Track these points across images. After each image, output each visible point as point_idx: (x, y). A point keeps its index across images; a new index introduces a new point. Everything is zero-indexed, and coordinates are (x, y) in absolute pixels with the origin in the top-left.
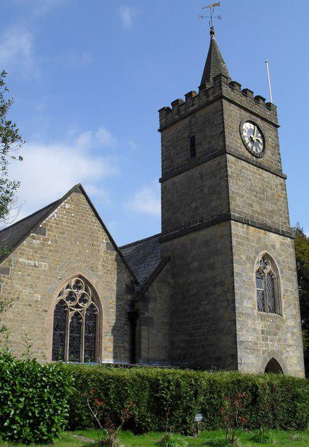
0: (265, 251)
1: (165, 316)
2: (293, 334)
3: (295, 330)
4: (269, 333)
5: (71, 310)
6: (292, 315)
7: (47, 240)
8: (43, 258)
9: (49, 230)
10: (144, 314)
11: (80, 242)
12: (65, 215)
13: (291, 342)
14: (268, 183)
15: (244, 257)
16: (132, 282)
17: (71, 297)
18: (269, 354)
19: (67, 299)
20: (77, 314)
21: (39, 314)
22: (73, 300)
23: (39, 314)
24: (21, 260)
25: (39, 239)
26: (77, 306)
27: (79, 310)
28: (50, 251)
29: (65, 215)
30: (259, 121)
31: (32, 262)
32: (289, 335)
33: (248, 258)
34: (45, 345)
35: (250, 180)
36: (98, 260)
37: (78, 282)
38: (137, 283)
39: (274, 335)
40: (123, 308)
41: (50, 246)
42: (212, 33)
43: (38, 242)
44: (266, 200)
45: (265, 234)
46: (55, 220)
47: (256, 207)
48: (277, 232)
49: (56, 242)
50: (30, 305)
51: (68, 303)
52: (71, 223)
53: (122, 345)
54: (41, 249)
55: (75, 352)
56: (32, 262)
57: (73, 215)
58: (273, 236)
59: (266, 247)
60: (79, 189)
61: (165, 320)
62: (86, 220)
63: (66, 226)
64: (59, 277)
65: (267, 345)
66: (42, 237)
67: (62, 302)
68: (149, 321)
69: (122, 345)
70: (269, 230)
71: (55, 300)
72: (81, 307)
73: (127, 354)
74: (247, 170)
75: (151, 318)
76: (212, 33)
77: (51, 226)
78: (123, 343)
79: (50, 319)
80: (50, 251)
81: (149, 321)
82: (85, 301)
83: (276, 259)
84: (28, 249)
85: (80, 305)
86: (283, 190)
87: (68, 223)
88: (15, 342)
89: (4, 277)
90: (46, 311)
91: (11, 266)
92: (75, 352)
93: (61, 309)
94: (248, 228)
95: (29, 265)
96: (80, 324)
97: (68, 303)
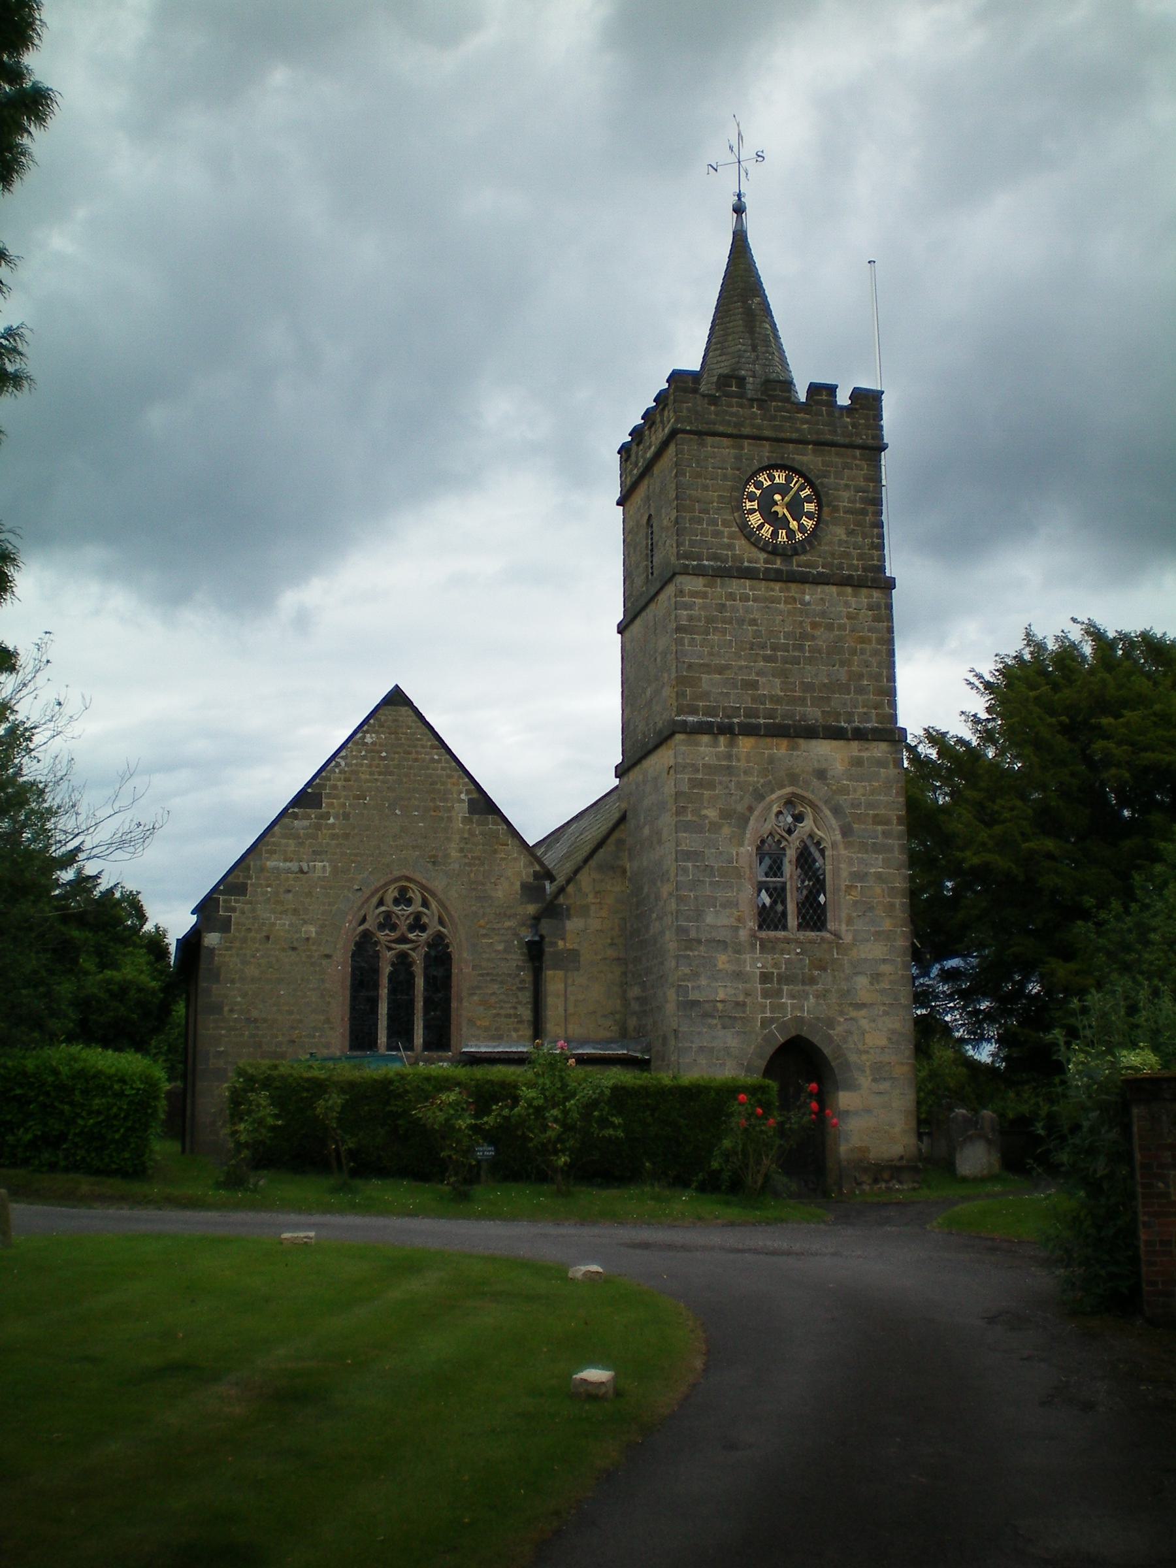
0: (788, 790)
1: (612, 944)
3: (886, 968)
4: (784, 979)
5: (390, 949)
7: (327, 816)
8: (317, 854)
9: (329, 796)
10: (554, 944)
12: (364, 757)
13: (864, 996)
14: (823, 614)
15: (712, 814)
16: (536, 875)
17: (388, 922)
19: (381, 927)
20: (403, 957)
21: (313, 964)
22: (394, 927)
23: (313, 964)
24: (270, 864)
25: (308, 817)
26: (403, 940)
27: (407, 946)
29: (364, 757)
30: (808, 458)
31: (294, 866)
33: (726, 814)
34: (328, 1021)
35: (753, 622)
36: (449, 839)
37: (403, 891)
38: (550, 876)
39: (803, 983)
40: (516, 935)
41: (333, 826)
42: (739, 209)
43: (306, 823)
44: (810, 661)
48: (836, 734)
49: (346, 816)
50: (294, 949)
51: (382, 936)
52: (380, 773)
53: (512, 1012)
54: (315, 837)
55: (401, 1031)
56: (294, 866)
57: (384, 754)
58: (824, 751)
59: (793, 779)
61: (611, 953)
62: (416, 760)
63: (367, 781)
64: (356, 887)
66: (313, 812)
67: (366, 935)
68: (570, 960)
69: (512, 1012)
70: (810, 733)
71: (349, 929)
72: (412, 941)
73: (529, 1032)
75: (574, 955)
76: (739, 209)
77: (335, 787)
78: (515, 1008)
79: (339, 970)
81: (570, 960)
84: (284, 841)
85: (411, 936)
86: (877, 619)
87: (371, 774)
88: (265, 1020)
89: (236, 901)
90: (328, 956)
91: (250, 878)
92: (401, 1031)
93: (364, 947)
95: (289, 871)
96: (412, 976)
97: (382, 936)
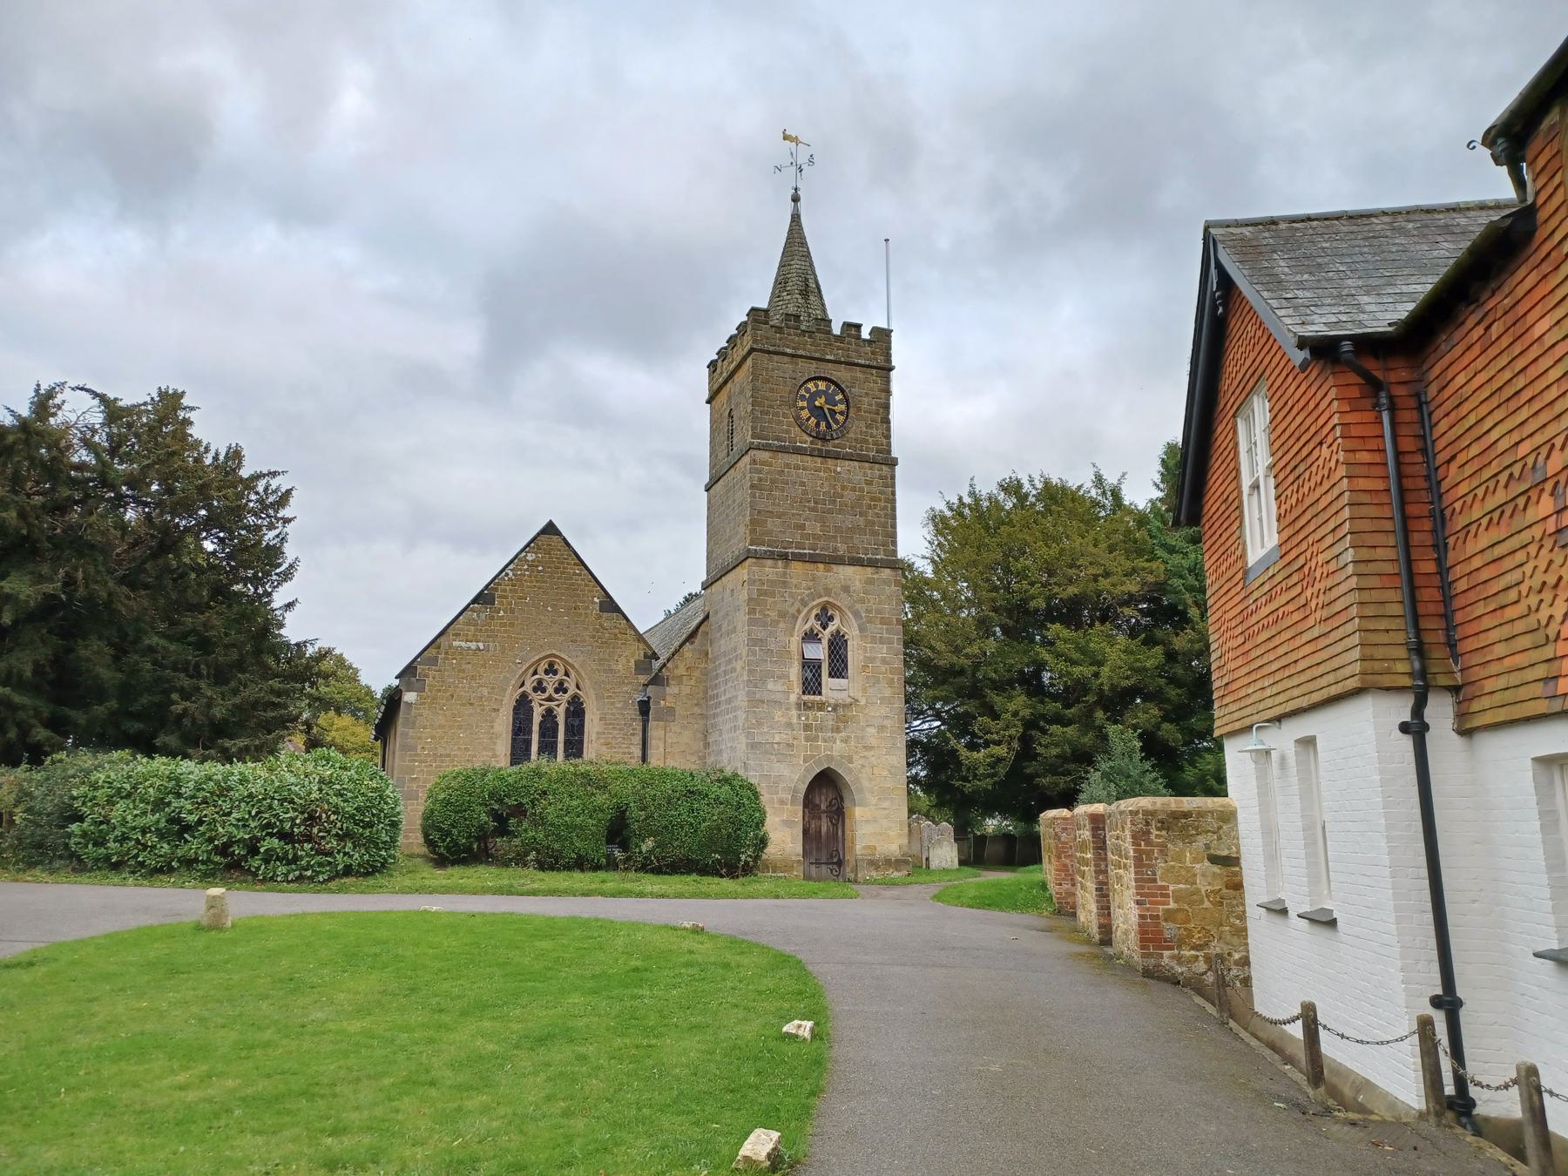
2: (882, 728)
3: (887, 723)
5: (541, 705)
6: (882, 699)
11: (553, 606)
12: (527, 570)
18: (818, 762)
20: (549, 711)
24: (455, 643)
28: (504, 625)
29: (527, 570)
32: (872, 730)
33: (782, 614)
35: (803, 484)
42: (796, 199)
45: (828, 571)
46: (510, 579)
47: (814, 528)
49: (512, 611)
50: (471, 704)
52: (537, 582)
56: (473, 645)
57: (540, 568)
59: (828, 592)
60: (550, 529)
63: (528, 587)
65: (818, 747)
67: (524, 696)
69: (626, 750)
74: (797, 467)
76: (796, 199)
80: (504, 625)
82: (565, 691)
83: (849, 608)
84: (466, 628)
85: (556, 696)
94: (786, 567)
